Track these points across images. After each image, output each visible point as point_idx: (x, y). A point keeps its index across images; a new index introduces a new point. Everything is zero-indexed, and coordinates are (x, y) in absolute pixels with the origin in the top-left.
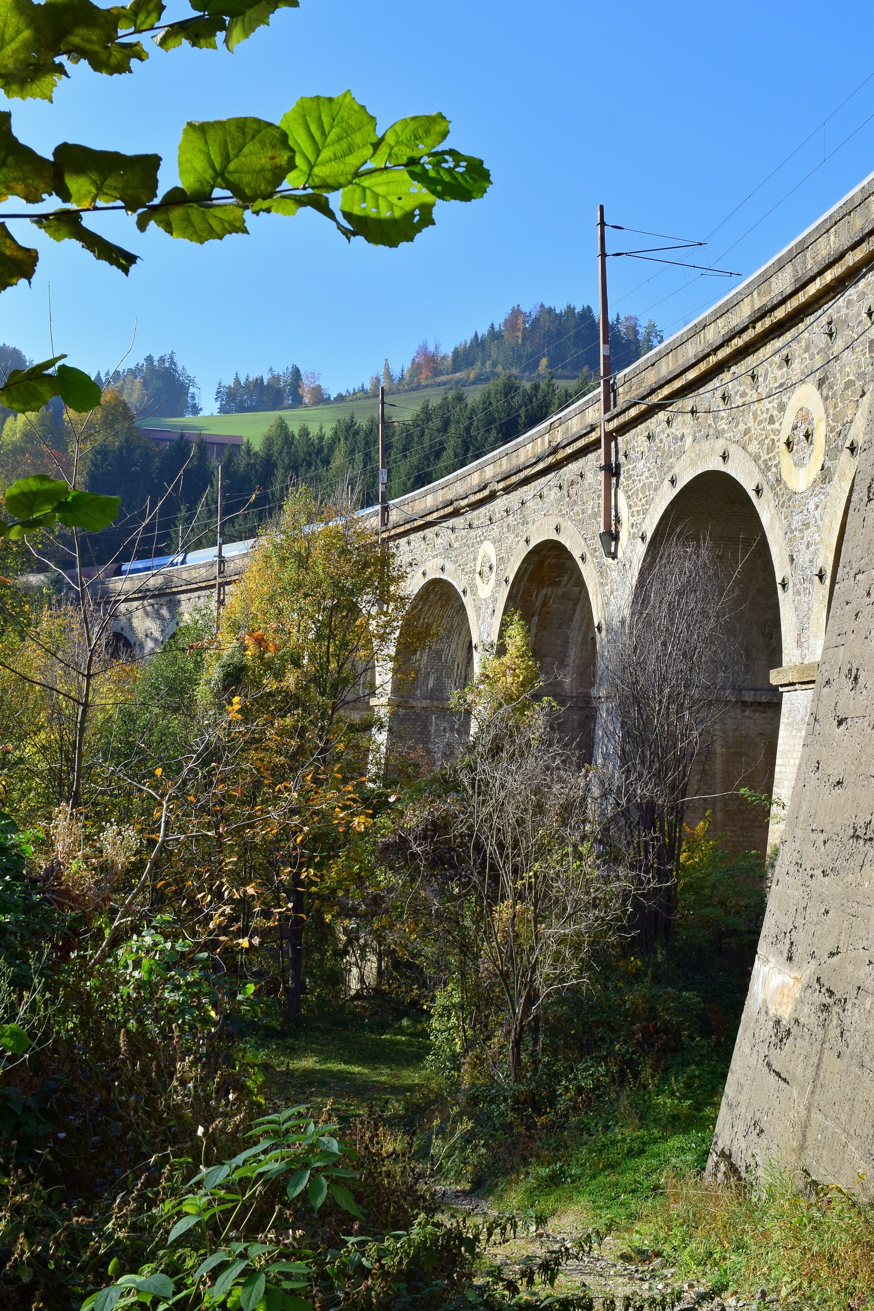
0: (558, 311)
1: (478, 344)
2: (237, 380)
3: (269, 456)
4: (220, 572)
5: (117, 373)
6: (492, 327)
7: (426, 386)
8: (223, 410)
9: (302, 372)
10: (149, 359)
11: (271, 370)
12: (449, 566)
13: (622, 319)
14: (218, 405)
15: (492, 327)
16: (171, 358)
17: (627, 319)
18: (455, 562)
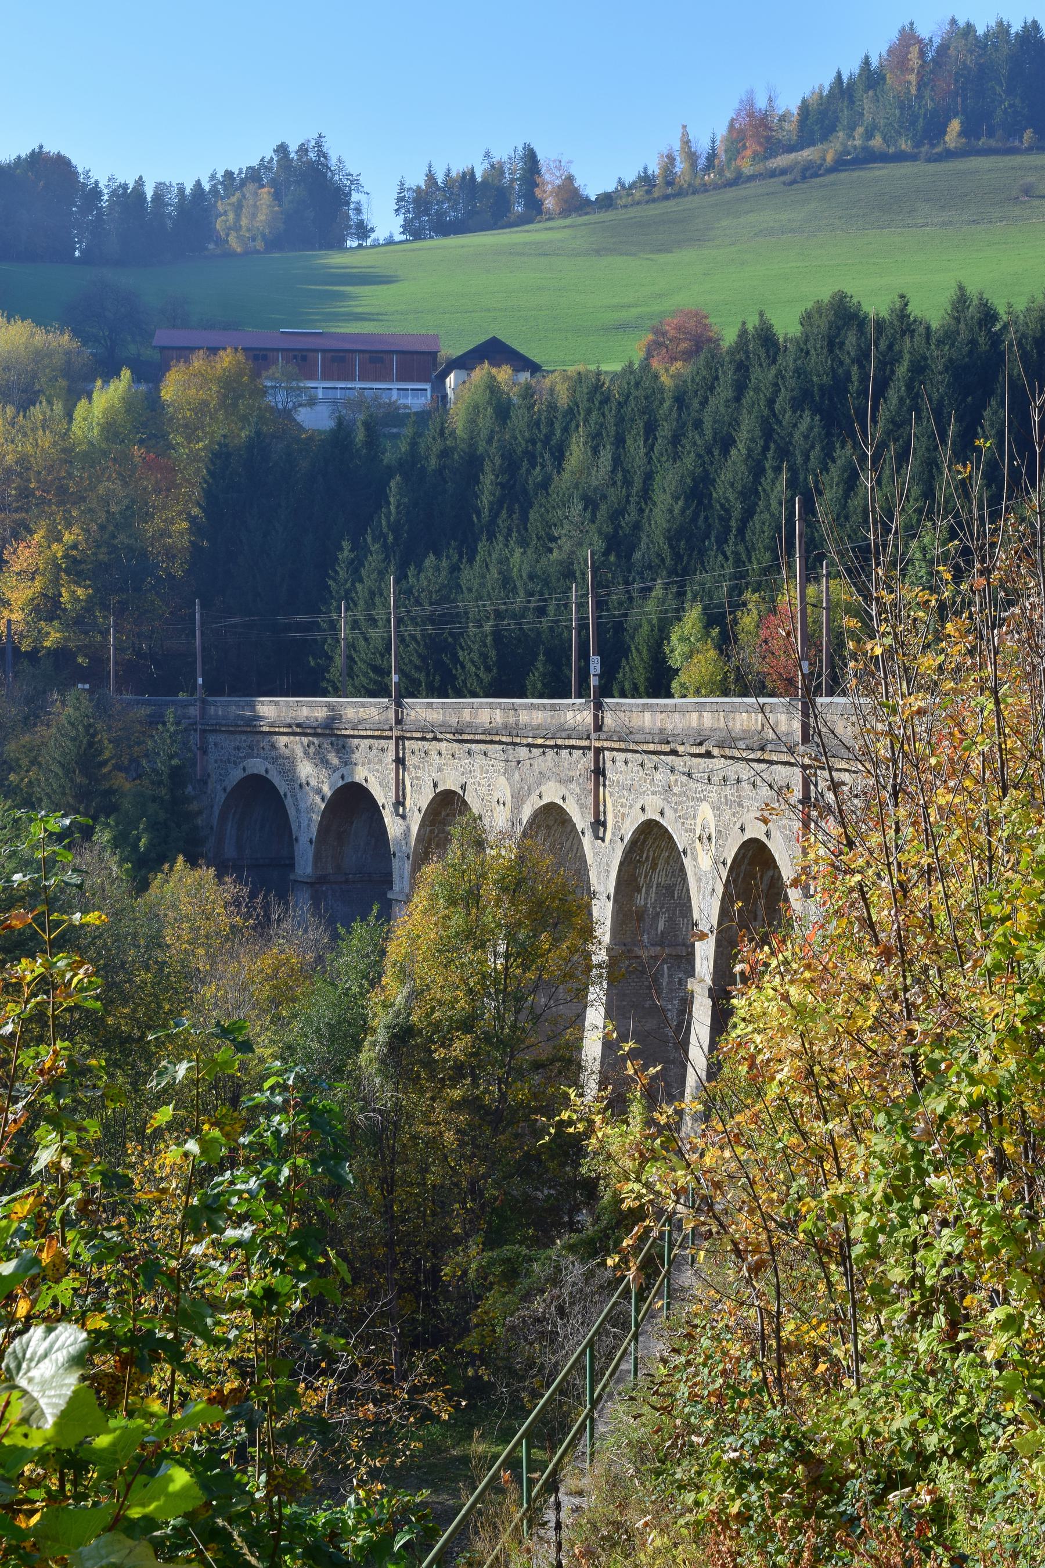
0: (981, 31)
1: (843, 91)
2: (431, 178)
3: (472, 444)
4: (399, 722)
5: (229, 174)
6: (867, 62)
8: (414, 231)
9: (540, 156)
10: (282, 149)
11: (487, 155)
12: (668, 812)
14: (400, 220)
15: (867, 62)
16: (319, 145)
18: (676, 811)
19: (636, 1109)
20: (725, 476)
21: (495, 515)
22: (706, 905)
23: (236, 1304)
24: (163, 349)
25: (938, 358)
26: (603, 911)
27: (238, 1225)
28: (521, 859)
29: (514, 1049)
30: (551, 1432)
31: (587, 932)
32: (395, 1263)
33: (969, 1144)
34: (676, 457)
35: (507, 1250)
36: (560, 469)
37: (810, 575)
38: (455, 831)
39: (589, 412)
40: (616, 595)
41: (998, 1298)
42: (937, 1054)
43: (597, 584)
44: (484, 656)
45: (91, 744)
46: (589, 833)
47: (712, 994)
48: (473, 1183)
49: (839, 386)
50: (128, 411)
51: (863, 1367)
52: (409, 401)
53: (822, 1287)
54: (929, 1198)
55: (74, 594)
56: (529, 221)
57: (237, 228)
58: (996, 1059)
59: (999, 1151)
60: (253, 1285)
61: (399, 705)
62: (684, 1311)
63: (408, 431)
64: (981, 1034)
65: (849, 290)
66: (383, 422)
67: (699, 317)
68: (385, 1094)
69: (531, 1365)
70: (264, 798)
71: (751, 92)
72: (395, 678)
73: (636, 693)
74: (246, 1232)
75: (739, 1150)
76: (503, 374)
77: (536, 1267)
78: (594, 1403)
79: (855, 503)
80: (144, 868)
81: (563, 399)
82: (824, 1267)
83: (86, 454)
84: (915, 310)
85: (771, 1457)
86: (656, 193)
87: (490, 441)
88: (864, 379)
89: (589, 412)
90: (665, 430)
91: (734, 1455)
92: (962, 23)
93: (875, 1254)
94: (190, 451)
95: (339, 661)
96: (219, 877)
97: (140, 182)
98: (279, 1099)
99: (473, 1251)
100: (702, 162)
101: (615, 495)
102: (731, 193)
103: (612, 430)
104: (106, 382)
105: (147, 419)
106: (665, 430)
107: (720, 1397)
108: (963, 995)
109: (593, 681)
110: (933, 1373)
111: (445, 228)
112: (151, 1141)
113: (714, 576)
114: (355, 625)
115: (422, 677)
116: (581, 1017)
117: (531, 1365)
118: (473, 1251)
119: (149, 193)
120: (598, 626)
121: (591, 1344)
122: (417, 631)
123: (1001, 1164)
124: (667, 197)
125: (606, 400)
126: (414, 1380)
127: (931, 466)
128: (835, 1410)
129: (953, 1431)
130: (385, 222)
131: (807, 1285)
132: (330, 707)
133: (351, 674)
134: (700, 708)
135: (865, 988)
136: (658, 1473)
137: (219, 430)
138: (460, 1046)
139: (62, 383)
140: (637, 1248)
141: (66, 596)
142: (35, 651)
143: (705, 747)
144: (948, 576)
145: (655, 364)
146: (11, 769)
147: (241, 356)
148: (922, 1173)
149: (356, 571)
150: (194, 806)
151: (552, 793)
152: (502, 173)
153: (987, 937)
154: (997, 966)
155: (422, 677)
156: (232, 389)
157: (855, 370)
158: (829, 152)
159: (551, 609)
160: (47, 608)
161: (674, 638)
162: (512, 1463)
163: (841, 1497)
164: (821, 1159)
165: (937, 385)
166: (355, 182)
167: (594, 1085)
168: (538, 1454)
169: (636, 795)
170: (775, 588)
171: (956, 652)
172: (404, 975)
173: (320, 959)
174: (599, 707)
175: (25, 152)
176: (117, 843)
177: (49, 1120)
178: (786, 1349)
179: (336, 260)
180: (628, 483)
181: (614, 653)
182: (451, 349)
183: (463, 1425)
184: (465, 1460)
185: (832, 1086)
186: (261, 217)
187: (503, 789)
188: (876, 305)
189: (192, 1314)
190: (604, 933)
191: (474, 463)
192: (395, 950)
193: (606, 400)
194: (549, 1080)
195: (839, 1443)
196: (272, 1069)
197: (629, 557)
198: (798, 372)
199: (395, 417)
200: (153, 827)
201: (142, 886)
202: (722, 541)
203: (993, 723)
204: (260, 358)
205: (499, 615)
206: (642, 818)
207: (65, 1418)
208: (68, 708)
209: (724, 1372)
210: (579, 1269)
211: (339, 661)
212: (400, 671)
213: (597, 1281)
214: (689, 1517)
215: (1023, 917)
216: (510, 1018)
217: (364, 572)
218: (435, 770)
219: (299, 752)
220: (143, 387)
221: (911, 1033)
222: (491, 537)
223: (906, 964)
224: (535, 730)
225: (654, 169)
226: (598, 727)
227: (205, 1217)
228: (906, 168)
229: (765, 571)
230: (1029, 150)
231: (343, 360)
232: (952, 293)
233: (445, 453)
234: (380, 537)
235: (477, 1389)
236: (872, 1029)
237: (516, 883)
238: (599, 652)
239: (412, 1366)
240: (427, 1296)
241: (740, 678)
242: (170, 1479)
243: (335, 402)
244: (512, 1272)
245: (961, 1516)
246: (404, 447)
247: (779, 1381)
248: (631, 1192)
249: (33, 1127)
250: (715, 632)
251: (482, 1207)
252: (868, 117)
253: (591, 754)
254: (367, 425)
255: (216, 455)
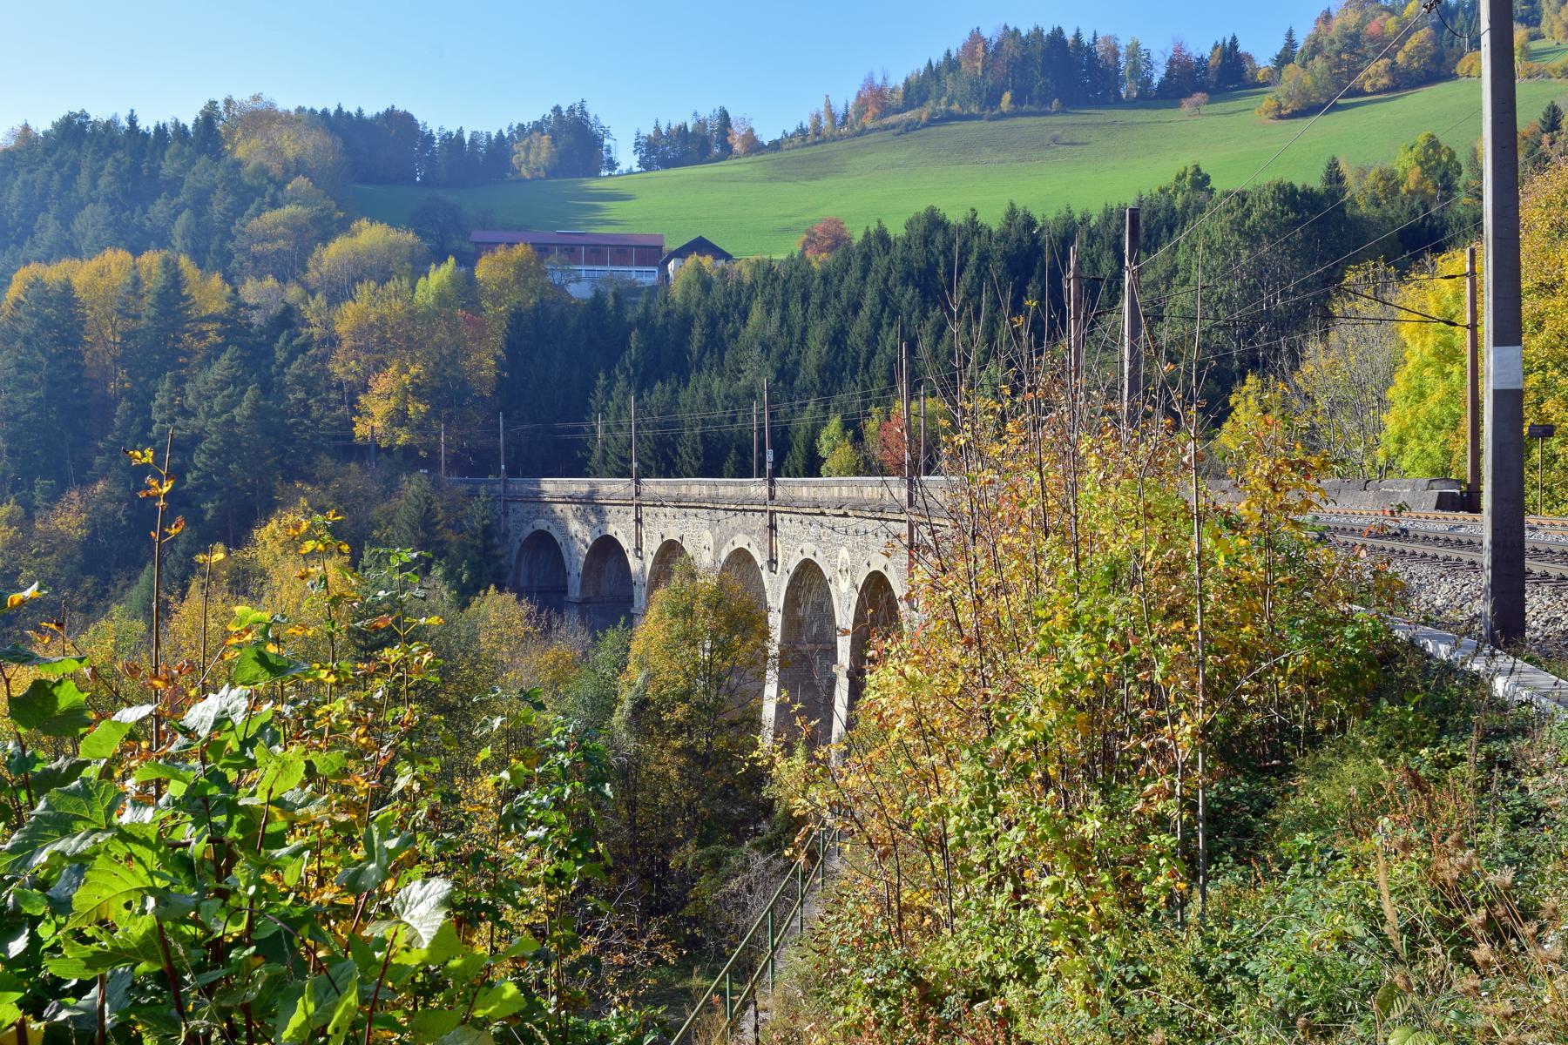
0: (1024, 34)
1: (933, 73)
2: (657, 129)
3: (686, 309)
4: (638, 494)
5: (521, 126)
6: (948, 53)
7: (872, 131)
8: (646, 165)
10: (557, 109)
13: (1099, 39)
14: (637, 158)
15: (948, 53)
16: (582, 107)
17: (1105, 39)
19: (799, 752)
20: (856, 329)
21: (702, 354)
22: (844, 616)
23: (534, 882)
24: (476, 244)
25: (997, 250)
26: (775, 620)
27: (534, 828)
28: (720, 585)
29: (720, 712)
30: (744, 971)
31: (765, 634)
32: (637, 858)
33: (1025, 771)
34: (823, 316)
35: (713, 848)
36: (745, 324)
37: (913, 396)
38: (677, 567)
39: (764, 286)
40: (783, 409)
41: (1046, 871)
42: (1004, 710)
43: (770, 402)
44: (695, 450)
45: (429, 510)
46: (766, 568)
47: (850, 675)
48: (689, 804)
49: (931, 270)
50: (453, 285)
51: (956, 921)
52: (644, 279)
53: (928, 867)
54: (1000, 806)
55: (417, 409)
56: (724, 159)
57: (527, 162)
58: (1043, 713)
59: (1046, 774)
60: (544, 868)
61: (638, 483)
62: (833, 886)
63: (643, 299)
64: (1033, 696)
65: (937, 205)
66: (626, 293)
67: (838, 223)
68: (630, 744)
69: (729, 926)
70: (546, 545)
71: (872, 74)
72: (635, 465)
73: (797, 474)
74: (541, 832)
75: (872, 776)
76: (707, 261)
77: (732, 859)
78: (774, 949)
79: (943, 347)
80: (465, 594)
81: (747, 279)
82: (929, 854)
83: (425, 315)
84: (982, 218)
85: (895, 981)
86: (809, 141)
87: (698, 305)
88: (949, 264)
89: (764, 286)
90: (815, 299)
91: (870, 981)
92: (1011, 28)
93: (963, 843)
94: (496, 314)
95: (597, 454)
96: (519, 599)
97: (461, 131)
98: (562, 743)
99: (690, 849)
100: (839, 119)
101: (782, 342)
102: (858, 141)
103: (780, 298)
104: (438, 266)
105: (466, 291)
106: (815, 299)
107: (860, 943)
108: (1020, 670)
109: (768, 466)
110: (1003, 923)
111: (667, 163)
112: (471, 774)
113: (849, 396)
114: (608, 429)
115: (653, 464)
116: (761, 691)
117: (729, 926)
118: (690, 849)
119: (467, 139)
120: (772, 430)
121: (771, 909)
122: (649, 433)
123: (1047, 782)
124: (816, 143)
125: (776, 279)
126: (651, 936)
127: (993, 323)
128: (937, 950)
129: (1016, 962)
130: (627, 159)
131: (918, 867)
132: (591, 484)
133: (605, 462)
134: (839, 485)
135: (955, 666)
136: (819, 994)
137: (514, 299)
138: (681, 711)
139: (408, 266)
140: (803, 843)
141: (411, 410)
142: (391, 447)
143: (843, 509)
144: (1008, 392)
145: (808, 255)
146: (374, 527)
147: (529, 248)
148: (994, 790)
149: (608, 393)
150: (499, 552)
151: (741, 541)
152: (705, 126)
153: (1036, 631)
154: (1043, 651)
155: (653, 464)
156: (522, 269)
157: (941, 258)
158: (923, 113)
159: (740, 419)
160: (399, 418)
161: (823, 437)
162: (720, 991)
163: (942, 1008)
164: (927, 782)
165: (996, 269)
166: (607, 132)
167: (770, 737)
168: (736, 986)
169: (797, 543)
170: (889, 403)
171: (1013, 443)
172: (642, 664)
173: (585, 654)
174: (772, 483)
175: (382, 110)
176: (447, 576)
177: (406, 757)
178: (904, 909)
179: (594, 184)
180: (790, 334)
181: (782, 446)
182: (672, 244)
183: (685, 968)
184: (686, 992)
185: (933, 733)
186: (543, 155)
187: (708, 538)
188: (955, 216)
189: (504, 890)
190: (776, 634)
191: (687, 322)
192: (636, 648)
193: (776, 279)
194: (740, 734)
195: (941, 972)
196: (557, 725)
197: (791, 383)
198: (903, 260)
199: (635, 290)
200: (471, 566)
201: (465, 605)
202: (854, 372)
203: (1039, 489)
204: (543, 250)
205: (705, 422)
206: (801, 558)
207: (436, 942)
208: (414, 486)
209: (862, 926)
210: (762, 861)
211: (597, 454)
212: (638, 460)
213: (774, 868)
214: (840, 1024)
215: (1060, 617)
216: (713, 692)
217: (614, 394)
218: (662, 527)
219: (570, 515)
220: (463, 270)
221: (986, 696)
222: (699, 370)
223: (983, 651)
224: (730, 499)
225: (807, 124)
226: (772, 497)
227: (513, 821)
228: (975, 125)
229: (884, 393)
230: (1056, 113)
231: (598, 251)
232: (1005, 208)
233: (668, 314)
234: (624, 370)
235: (694, 943)
236: (959, 694)
237: (717, 603)
238: (772, 447)
239: (649, 927)
240: (658, 880)
241: (867, 464)
242: (504, 990)
243: (593, 280)
244: (716, 863)
245: (1023, 1019)
246: (640, 310)
247: (899, 931)
248: (799, 805)
249: (393, 762)
250: (850, 433)
251: (696, 820)
252: (949, 90)
253: (767, 515)
254: (615, 295)
255: (513, 315)
